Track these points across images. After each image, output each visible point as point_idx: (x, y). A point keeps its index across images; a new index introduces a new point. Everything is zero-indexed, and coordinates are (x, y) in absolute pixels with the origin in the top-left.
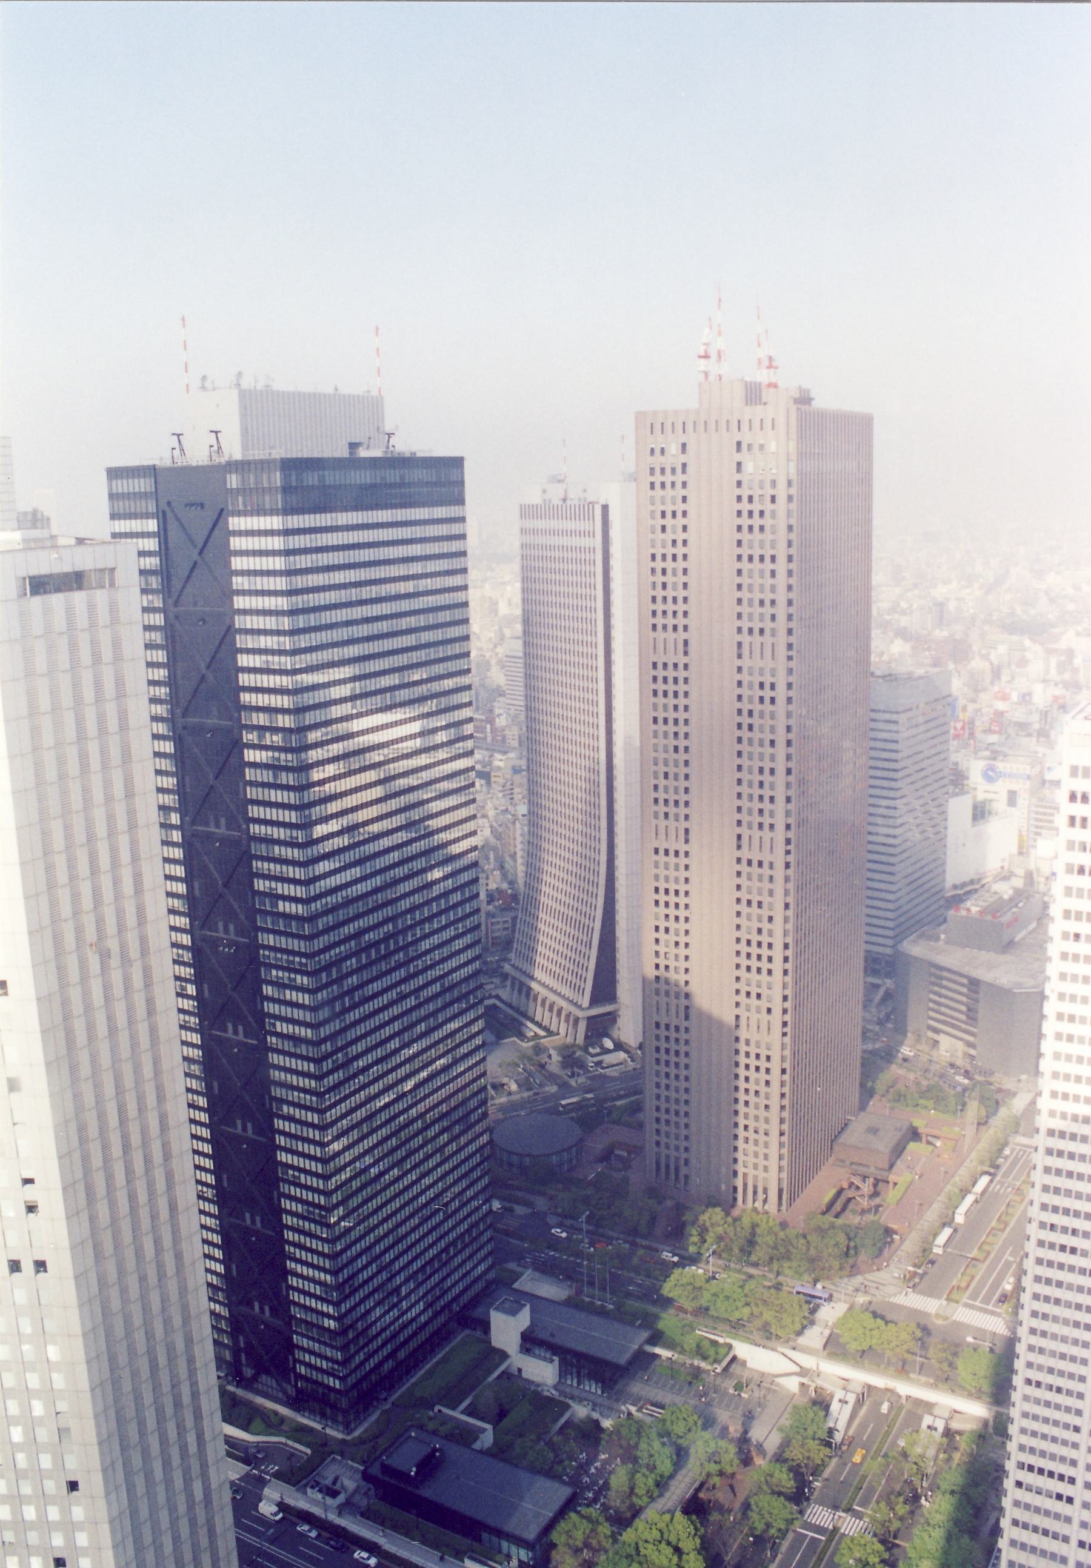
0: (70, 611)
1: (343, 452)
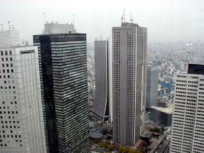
0: (28, 56)
1: (68, 33)
